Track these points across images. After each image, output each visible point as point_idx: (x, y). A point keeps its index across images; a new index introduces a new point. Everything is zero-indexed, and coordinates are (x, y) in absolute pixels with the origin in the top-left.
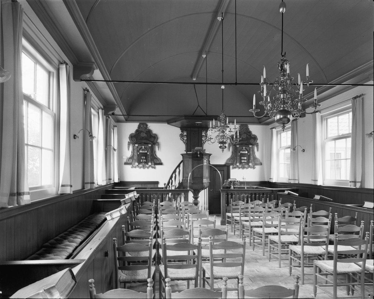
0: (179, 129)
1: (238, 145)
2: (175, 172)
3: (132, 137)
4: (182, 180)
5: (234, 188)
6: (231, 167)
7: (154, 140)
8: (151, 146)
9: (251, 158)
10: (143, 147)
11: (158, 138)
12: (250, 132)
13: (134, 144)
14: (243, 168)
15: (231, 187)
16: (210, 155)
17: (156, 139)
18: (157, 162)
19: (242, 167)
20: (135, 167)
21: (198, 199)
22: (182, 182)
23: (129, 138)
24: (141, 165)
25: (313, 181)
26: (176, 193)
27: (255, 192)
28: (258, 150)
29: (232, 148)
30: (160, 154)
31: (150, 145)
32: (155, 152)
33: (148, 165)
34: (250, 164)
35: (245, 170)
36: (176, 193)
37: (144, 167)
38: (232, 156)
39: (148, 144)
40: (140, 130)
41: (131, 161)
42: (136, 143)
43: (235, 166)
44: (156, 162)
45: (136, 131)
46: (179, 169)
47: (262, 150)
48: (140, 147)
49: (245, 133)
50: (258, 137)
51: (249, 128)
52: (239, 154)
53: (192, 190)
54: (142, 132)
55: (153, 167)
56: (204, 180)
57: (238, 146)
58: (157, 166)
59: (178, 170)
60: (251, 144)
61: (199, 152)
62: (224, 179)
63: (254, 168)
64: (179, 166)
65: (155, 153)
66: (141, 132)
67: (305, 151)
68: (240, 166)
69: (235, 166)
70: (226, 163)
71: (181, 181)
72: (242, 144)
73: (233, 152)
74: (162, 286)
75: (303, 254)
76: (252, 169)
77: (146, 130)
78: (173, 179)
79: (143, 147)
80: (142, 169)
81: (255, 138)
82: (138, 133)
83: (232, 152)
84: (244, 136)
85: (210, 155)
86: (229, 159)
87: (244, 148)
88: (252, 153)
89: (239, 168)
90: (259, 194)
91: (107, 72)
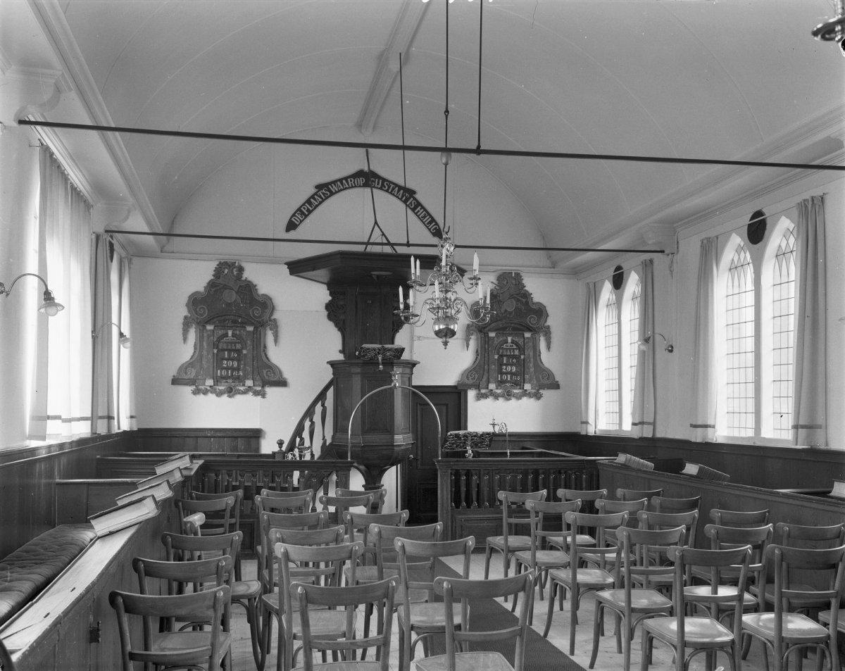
0: (325, 287)
1: (491, 330)
2: (309, 413)
3: (195, 301)
5: (476, 454)
6: (471, 394)
8: (253, 331)
9: (529, 369)
10: (230, 333)
12: (527, 295)
13: (201, 325)
14: (508, 396)
15: (466, 452)
16: (414, 365)
17: (268, 311)
18: (270, 378)
19: (503, 396)
20: (205, 392)
23: (187, 305)
25: (709, 424)
26: (317, 473)
27: (535, 467)
28: (549, 347)
29: (477, 339)
30: (277, 354)
31: (250, 329)
32: (265, 347)
33: (244, 385)
34: (527, 386)
35: (513, 401)
36: (317, 473)
39: (243, 325)
40: (220, 281)
41: (192, 373)
42: (208, 322)
43: (483, 391)
44: (266, 377)
45: (209, 283)
47: (321, 463)
48: (221, 332)
49: (512, 297)
50: (549, 310)
51: (524, 282)
52: (496, 357)
53: (362, 467)
55: (256, 393)
56: (396, 437)
57: (492, 335)
58: (270, 391)
59: (319, 408)
60: (529, 330)
61: (380, 358)
62: (447, 427)
63: (538, 396)
64: (321, 397)
65: (264, 351)
66: (225, 287)
67: (674, 350)
68: (499, 391)
69: (483, 391)
70: (458, 384)
71: (328, 442)
72: (504, 329)
73: (479, 351)
75: (781, 639)
76: (532, 400)
78: (306, 434)
81: (541, 312)
83: (477, 351)
84: (510, 306)
85: (414, 365)
86: (468, 373)
88: (531, 354)
89: (496, 397)
90: (547, 473)
91: (121, 143)
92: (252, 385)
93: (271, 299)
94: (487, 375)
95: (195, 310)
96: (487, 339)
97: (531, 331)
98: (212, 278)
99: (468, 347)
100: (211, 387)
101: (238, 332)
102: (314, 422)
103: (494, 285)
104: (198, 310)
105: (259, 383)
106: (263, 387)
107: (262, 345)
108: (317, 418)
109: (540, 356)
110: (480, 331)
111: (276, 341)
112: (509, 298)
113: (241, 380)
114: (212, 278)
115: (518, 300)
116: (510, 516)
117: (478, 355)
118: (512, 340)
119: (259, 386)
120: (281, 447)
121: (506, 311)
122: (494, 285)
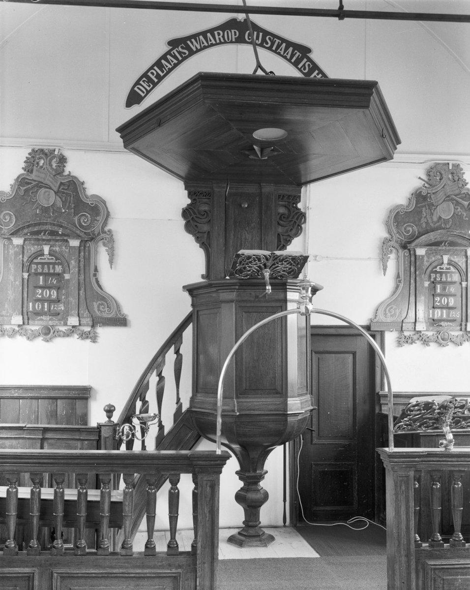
2: (156, 363)
4: (192, 400)
7: (94, 220)
10: (46, 249)
11: (108, 215)
17: (100, 219)
21: (262, 484)
22: (188, 411)
24: (35, 327)
31: (75, 243)
32: (96, 270)
33: (65, 324)
37: (48, 333)
38: (394, 292)
40: (33, 176)
46: (177, 352)
48: (33, 249)
49: (448, 198)
51: (465, 177)
54: (41, 187)
55: (84, 336)
56: (291, 401)
57: (421, 252)
58: (105, 333)
59: (171, 356)
61: (267, 274)
64: (175, 339)
65: (95, 275)
66: (40, 185)
71: (186, 406)
74: (274, 447)
77: (60, 179)
78: (151, 396)
79: (46, 249)
80: (39, 341)
82: (26, 191)
83: (398, 276)
87: (446, 259)
89: (426, 342)
92: (78, 324)
93: (104, 202)
98: (23, 172)
99: (385, 270)
100: (19, 326)
101: (57, 249)
102: (147, 402)
103: (423, 182)
105: (88, 321)
106: (93, 326)
108: (168, 371)
110: (404, 247)
111: (111, 261)
114: (23, 172)
119: (88, 325)
121: (440, 218)
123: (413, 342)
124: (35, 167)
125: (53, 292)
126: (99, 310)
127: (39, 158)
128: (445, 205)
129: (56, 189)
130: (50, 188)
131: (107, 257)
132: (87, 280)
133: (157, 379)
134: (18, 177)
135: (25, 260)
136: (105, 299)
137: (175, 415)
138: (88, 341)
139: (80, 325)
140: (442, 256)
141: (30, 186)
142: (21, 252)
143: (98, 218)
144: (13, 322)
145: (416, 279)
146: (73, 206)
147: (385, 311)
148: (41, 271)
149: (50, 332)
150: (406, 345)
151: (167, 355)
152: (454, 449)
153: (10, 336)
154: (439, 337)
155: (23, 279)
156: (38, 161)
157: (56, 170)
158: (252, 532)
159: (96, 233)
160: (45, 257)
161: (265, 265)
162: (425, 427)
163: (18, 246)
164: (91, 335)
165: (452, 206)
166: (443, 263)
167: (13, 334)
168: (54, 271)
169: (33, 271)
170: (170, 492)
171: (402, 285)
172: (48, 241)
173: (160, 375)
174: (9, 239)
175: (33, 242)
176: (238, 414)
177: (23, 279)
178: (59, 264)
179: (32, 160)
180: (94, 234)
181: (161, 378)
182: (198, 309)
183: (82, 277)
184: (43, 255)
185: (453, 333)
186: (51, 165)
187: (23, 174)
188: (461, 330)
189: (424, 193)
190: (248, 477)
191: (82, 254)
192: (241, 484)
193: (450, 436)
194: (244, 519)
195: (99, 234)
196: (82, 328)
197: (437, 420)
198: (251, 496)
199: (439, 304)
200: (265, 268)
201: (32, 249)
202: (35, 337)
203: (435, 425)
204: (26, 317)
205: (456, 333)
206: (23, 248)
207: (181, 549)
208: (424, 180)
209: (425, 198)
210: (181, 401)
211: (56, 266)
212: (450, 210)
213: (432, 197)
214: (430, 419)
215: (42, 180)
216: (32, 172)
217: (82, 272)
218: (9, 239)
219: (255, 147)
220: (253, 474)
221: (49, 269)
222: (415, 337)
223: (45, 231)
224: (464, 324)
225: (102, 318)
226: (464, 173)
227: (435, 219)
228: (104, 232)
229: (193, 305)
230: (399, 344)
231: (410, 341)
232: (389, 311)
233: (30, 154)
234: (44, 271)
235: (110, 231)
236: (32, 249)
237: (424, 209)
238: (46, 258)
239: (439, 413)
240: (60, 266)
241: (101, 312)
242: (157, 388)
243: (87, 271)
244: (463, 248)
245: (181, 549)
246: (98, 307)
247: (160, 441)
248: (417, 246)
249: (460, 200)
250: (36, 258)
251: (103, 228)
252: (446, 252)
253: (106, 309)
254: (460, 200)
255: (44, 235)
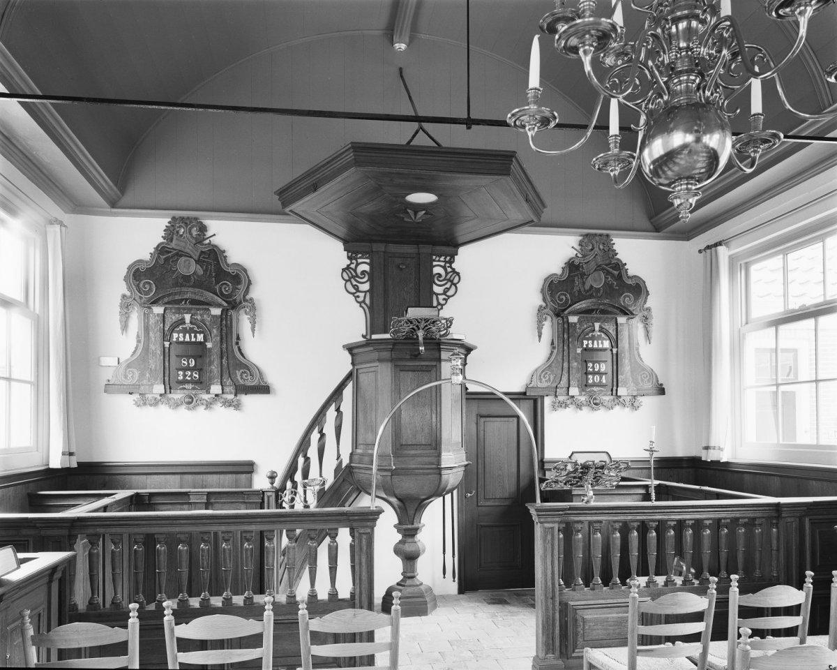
0: (339, 245)
1: (574, 313)
6: (548, 401)
7: (235, 289)
10: (188, 317)
11: (250, 283)
12: (619, 266)
17: (242, 287)
23: (126, 279)
24: (177, 395)
32: (238, 338)
33: (208, 392)
35: (601, 412)
37: (191, 402)
40: (173, 245)
42: (155, 303)
43: (561, 398)
46: (338, 410)
48: (175, 317)
49: (599, 268)
51: (615, 247)
52: (579, 351)
54: (181, 256)
55: (228, 404)
57: (573, 319)
58: (248, 400)
59: (331, 413)
61: (421, 334)
64: (337, 394)
65: (237, 343)
66: (180, 254)
68: (583, 399)
71: (346, 461)
73: (556, 343)
77: (201, 248)
78: (313, 452)
79: (188, 317)
80: (183, 410)
81: (638, 289)
82: (166, 260)
83: (552, 343)
87: (597, 325)
89: (579, 406)
92: (221, 392)
93: (245, 271)
94: (567, 375)
95: (138, 286)
96: (565, 326)
97: (626, 314)
98: (162, 240)
99: (540, 336)
100: (161, 395)
101: (199, 317)
102: (309, 458)
103: (576, 252)
104: (141, 285)
105: (232, 389)
106: (236, 395)
107: (234, 337)
108: (329, 428)
109: (638, 349)
110: (558, 315)
111: (253, 330)
112: (595, 270)
113: (202, 384)
114: (162, 240)
115: (608, 273)
116: (628, 617)
117: (554, 348)
118: (600, 327)
119: (231, 393)
120: (272, 483)
121: (592, 287)
122: (576, 252)
123: (566, 406)
124: (174, 236)
125: (192, 362)
126: (242, 378)
127: (180, 227)
128: (596, 274)
129: (196, 258)
130: (191, 257)
131: (250, 325)
132: (230, 348)
133: (319, 435)
134: (158, 246)
135: (166, 329)
136: (247, 367)
137: (335, 470)
138: (232, 409)
139: (223, 393)
140: (593, 324)
141: (170, 254)
142: (162, 321)
143: (239, 286)
144: (154, 391)
145: (569, 345)
146: (214, 274)
147: (540, 376)
148: (182, 339)
149: (193, 400)
150: (560, 409)
151: (328, 413)
152: (593, 504)
153: (151, 405)
154: (592, 401)
155: (164, 348)
156: (178, 229)
157: (196, 239)
158: (409, 582)
159: (238, 301)
160: (186, 325)
161: (417, 326)
162: (571, 485)
163: (158, 315)
164: (234, 404)
165: (603, 276)
166: (594, 331)
167: (155, 403)
168: (196, 339)
169: (175, 340)
170: (329, 545)
171: (555, 351)
172: (188, 311)
173: (321, 432)
174: (150, 308)
175: (173, 311)
176: (394, 468)
177: (164, 348)
178: (200, 333)
179: (172, 229)
180: (236, 303)
181: (322, 435)
182: (358, 367)
183: (224, 346)
184: (184, 323)
185: (604, 398)
186: (191, 234)
187: (162, 243)
188: (612, 395)
189: (577, 262)
190: (405, 530)
191: (224, 322)
192: (400, 537)
193: (591, 493)
194: (402, 571)
195: (240, 303)
196: (224, 396)
197: (580, 478)
198: (408, 548)
199: (591, 370)
200: (419, 329)
201: (172, 318)
202: (178, 406)
203: (579, 484)
204: (168, 387)
205: (607, 398)
206: (164, 317)
207: (341, 596)
208: (576, 250)
209: (577, 267)
210: (341, 457)
211: (198, 335)
212: (601, 279)
213: (584, 266)
214: (574, 477)
215: (183, 249)
216: (171, 240)
217: (224, 341)
218: (150, 308)
219: (409, 211)
220: (410, 526)
221: (190, 337)
222: (569, 402)
223: (186, 300)
224: (615, 388)
225: (244, 385)
226: (614, 244)
227: (587, 287)
228: (245, 300)
229: (353, 363)
230: (554, 408)
231: (564, 405)
232: (544, 377)
233: (170, 222)
234: (186, 340)
235: (251, 299)
236: (174, 317)
237: (576, 278)
238: (188, 325)
239: (581, 473)
240: (202, 335)
241: (245, 380)
242: (318, 445)
243: (229, 340)
244: (612, 316)
245: (341, 596)
246: (241, 375)
247: (321, 495)
248: (569, 313)
249: (611, 270)
250: (178, 326)
251: (244, 296)
252: (598, 320)
253: (249, 377)
254: (611, 270)
255: (185, 303)
